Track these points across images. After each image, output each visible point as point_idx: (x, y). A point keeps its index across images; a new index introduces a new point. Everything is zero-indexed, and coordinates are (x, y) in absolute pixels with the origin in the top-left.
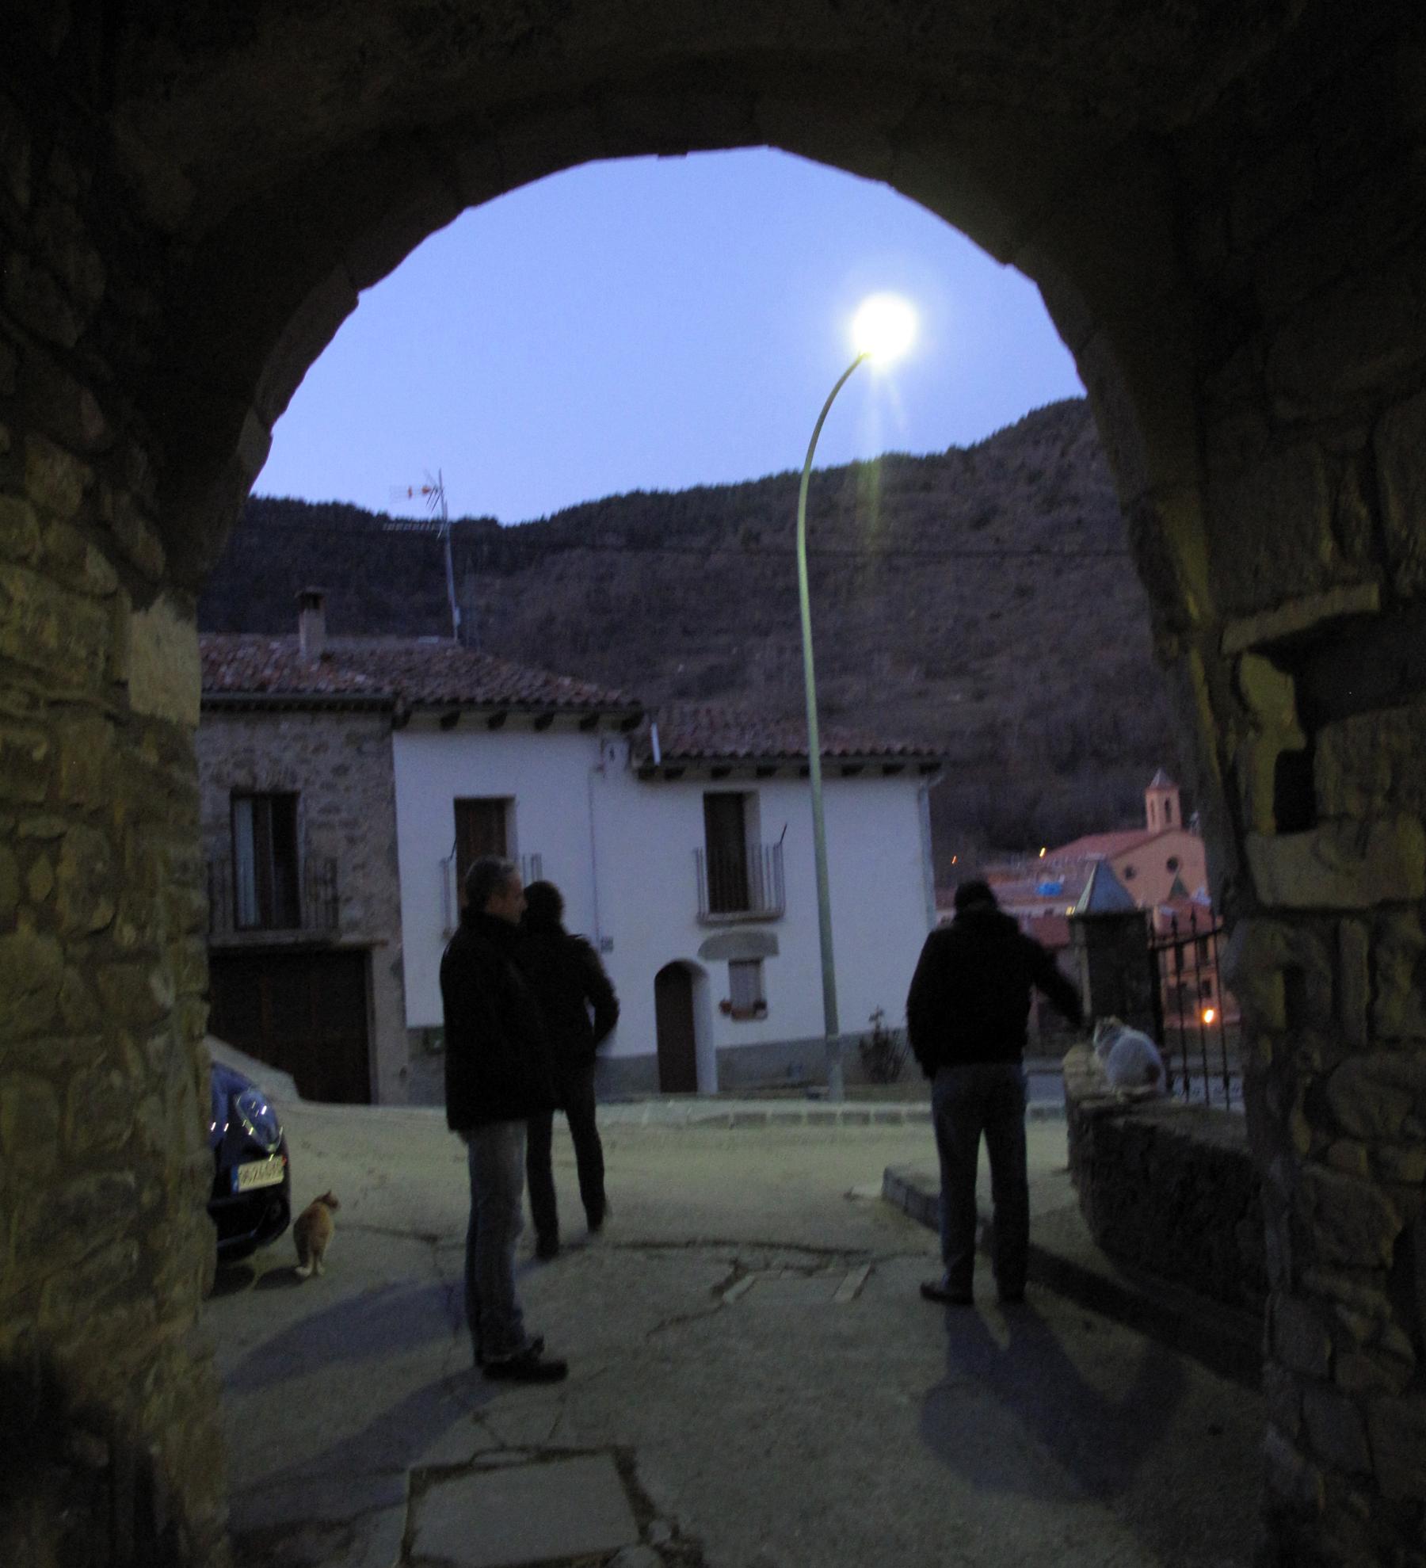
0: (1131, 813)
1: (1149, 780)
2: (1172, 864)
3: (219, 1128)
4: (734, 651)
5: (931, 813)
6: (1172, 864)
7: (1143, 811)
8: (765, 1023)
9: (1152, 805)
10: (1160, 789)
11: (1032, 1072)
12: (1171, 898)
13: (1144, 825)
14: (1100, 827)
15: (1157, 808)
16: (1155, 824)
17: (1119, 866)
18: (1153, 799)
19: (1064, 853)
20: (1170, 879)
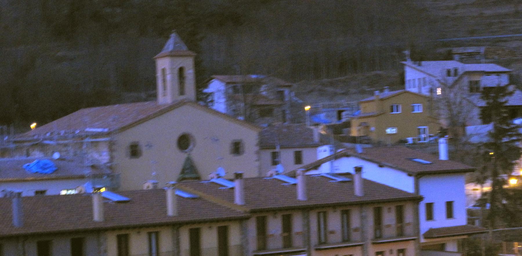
0: (139, 84)
1: (161, 47)
2: (184, 142)
3: (505, 112)
4: (488, 206)
5: (75, 111)
6: (184, 142)
7: (154, 86)
8: (245, 155)
9: (164, 70)
10: (172, 55)
11: (409, 66)
12: (181, 180)
13: (154, 96)
14: (100, 98)
15: (168, 77)
16: (166, 94)
17: (126, 139)
18: (164, 65)
19: (59, 126)
20: (180, 158)
